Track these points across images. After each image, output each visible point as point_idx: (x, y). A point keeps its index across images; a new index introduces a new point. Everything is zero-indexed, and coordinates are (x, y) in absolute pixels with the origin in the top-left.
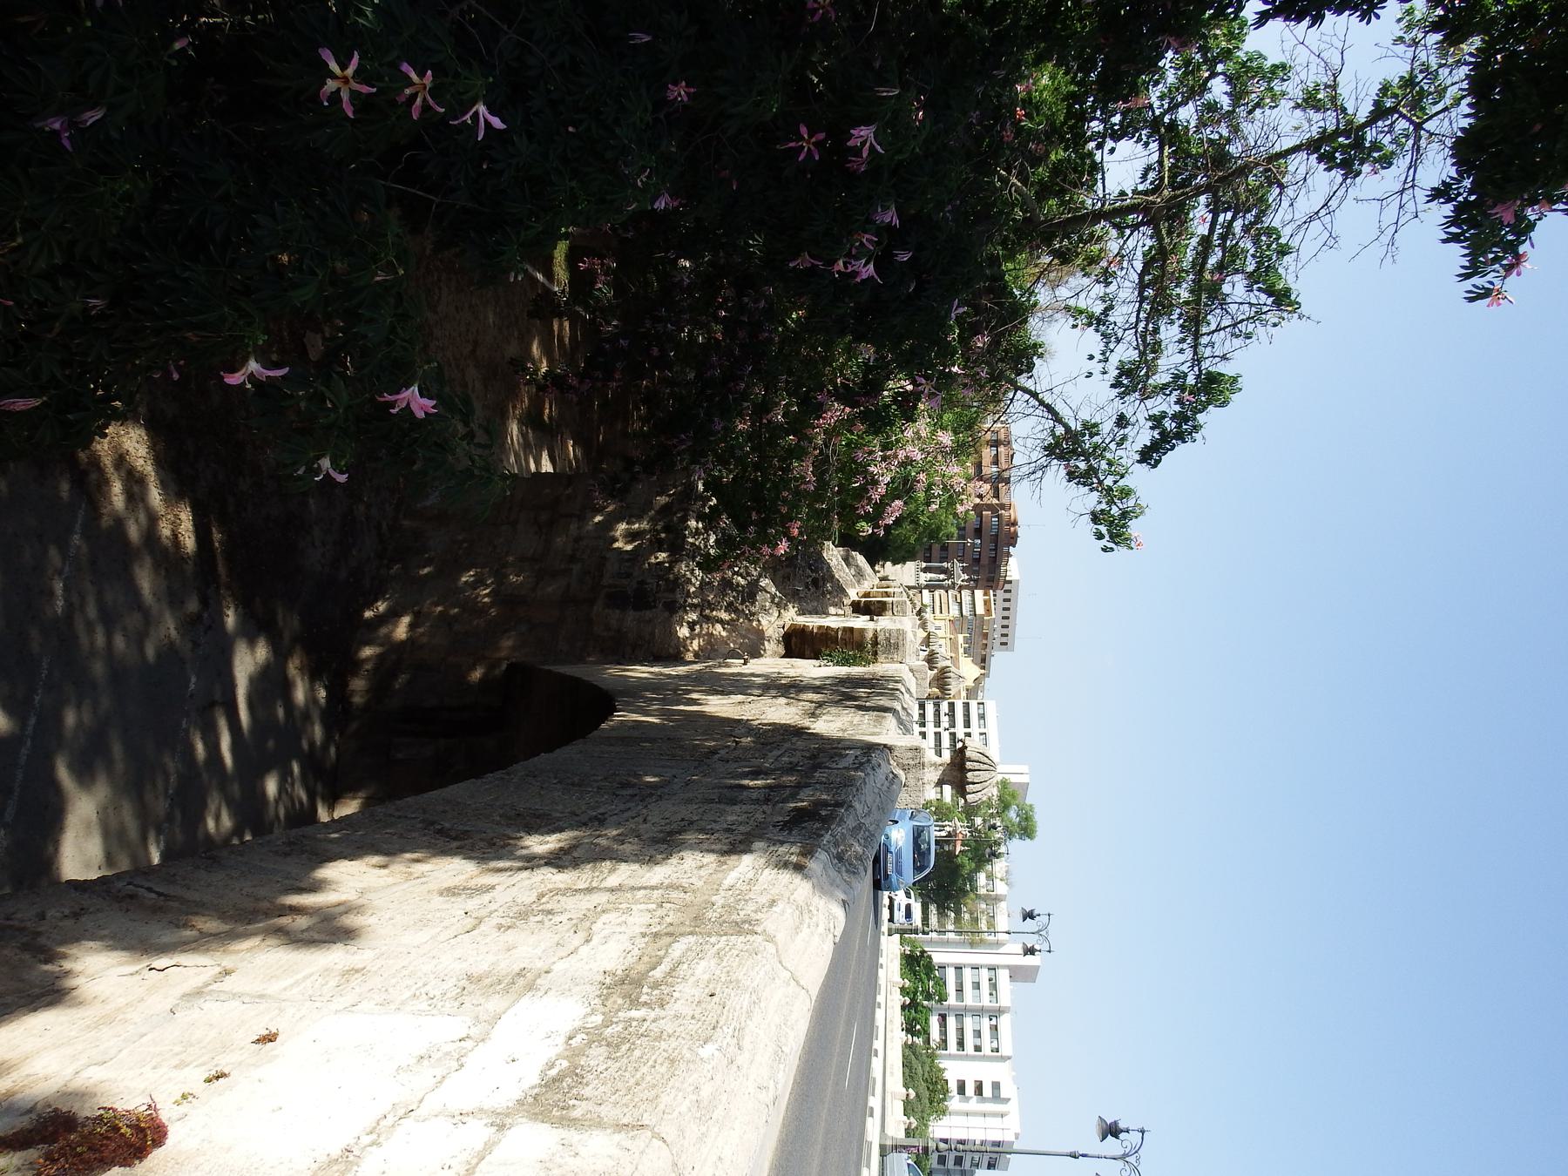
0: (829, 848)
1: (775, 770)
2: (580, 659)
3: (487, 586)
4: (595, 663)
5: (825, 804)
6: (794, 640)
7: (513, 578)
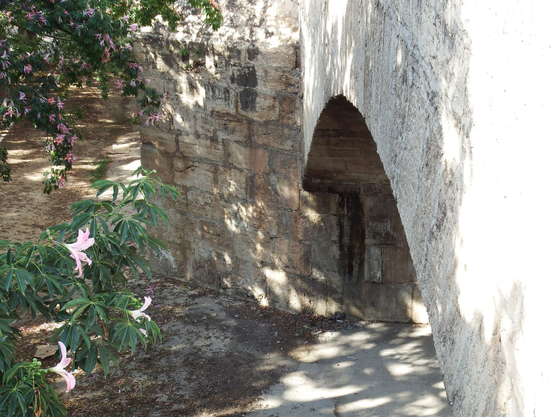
2: (299, 130)
4: (302, 118)
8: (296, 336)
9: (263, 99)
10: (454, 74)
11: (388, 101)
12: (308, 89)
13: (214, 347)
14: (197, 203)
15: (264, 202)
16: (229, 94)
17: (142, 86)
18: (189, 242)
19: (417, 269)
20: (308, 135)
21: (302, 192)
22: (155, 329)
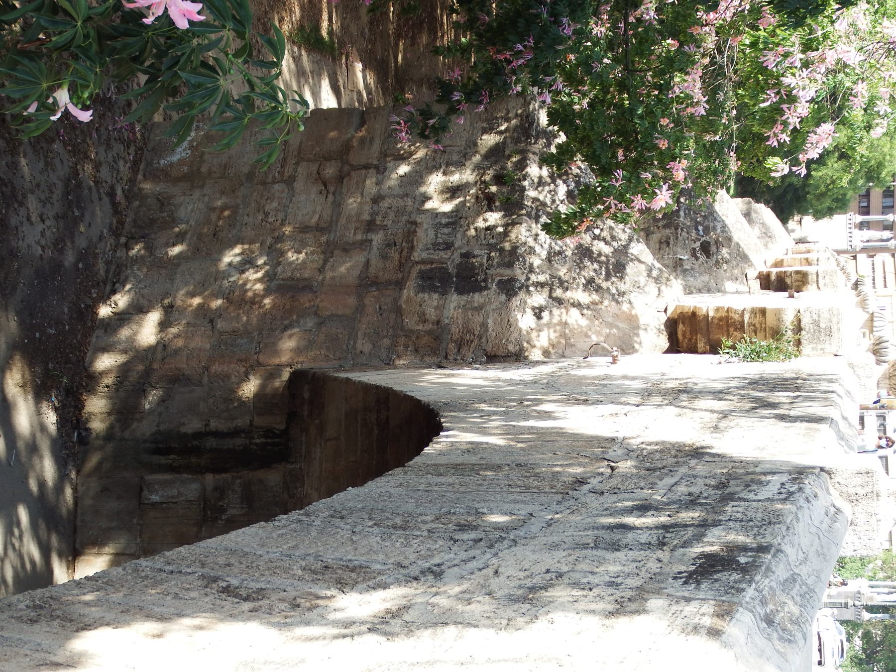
0: (754, 607)
1: (668, 504)
2: (389, 364)
3: (258, 268)
4: (408, 367)
5: (744, 549)
6: (681, 327)
7: (291, 256)
8: (48, 364)
9: (436, 304)
10: (469, 604)
11: (430, 502)
12: (453, 376)
13: (26, 228)
14: (267, 200)
15: (272, 308)
16: (444, 250)
17: (453, 110)
18: (202, 187)
19: (157, 558)
20: (380, 377)
21: (288, 369)
22: (37, 128)
